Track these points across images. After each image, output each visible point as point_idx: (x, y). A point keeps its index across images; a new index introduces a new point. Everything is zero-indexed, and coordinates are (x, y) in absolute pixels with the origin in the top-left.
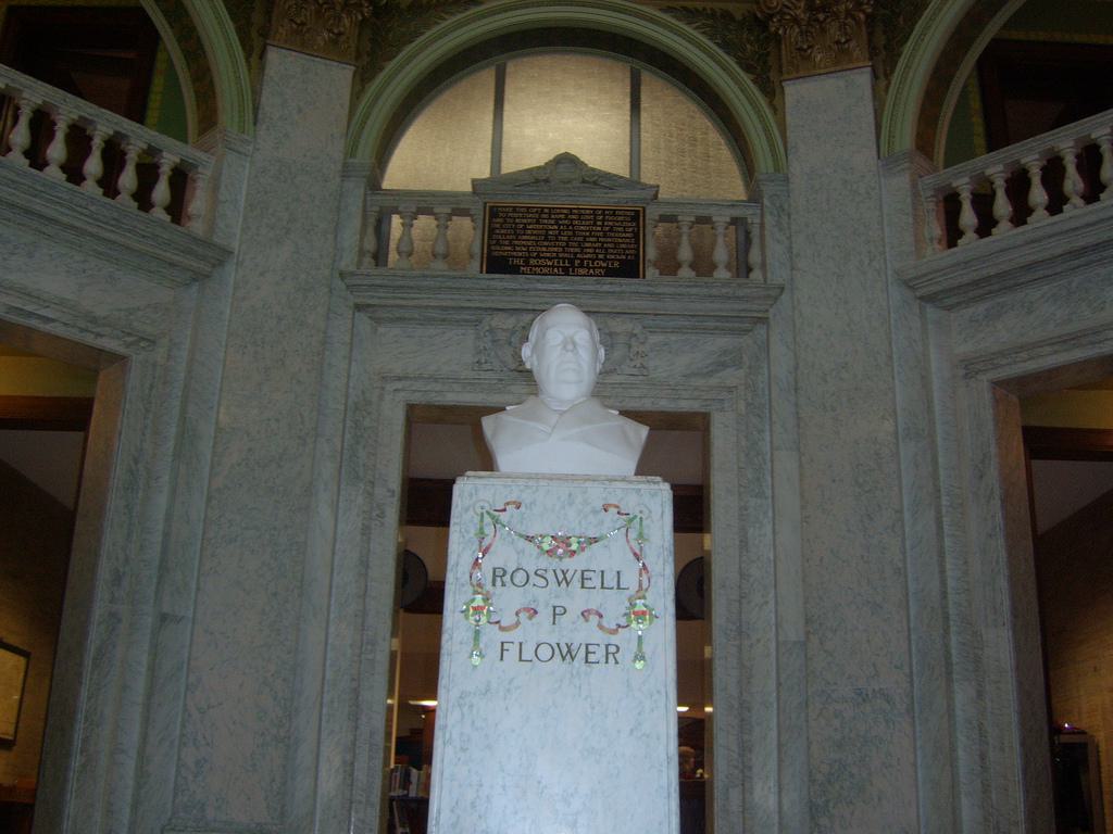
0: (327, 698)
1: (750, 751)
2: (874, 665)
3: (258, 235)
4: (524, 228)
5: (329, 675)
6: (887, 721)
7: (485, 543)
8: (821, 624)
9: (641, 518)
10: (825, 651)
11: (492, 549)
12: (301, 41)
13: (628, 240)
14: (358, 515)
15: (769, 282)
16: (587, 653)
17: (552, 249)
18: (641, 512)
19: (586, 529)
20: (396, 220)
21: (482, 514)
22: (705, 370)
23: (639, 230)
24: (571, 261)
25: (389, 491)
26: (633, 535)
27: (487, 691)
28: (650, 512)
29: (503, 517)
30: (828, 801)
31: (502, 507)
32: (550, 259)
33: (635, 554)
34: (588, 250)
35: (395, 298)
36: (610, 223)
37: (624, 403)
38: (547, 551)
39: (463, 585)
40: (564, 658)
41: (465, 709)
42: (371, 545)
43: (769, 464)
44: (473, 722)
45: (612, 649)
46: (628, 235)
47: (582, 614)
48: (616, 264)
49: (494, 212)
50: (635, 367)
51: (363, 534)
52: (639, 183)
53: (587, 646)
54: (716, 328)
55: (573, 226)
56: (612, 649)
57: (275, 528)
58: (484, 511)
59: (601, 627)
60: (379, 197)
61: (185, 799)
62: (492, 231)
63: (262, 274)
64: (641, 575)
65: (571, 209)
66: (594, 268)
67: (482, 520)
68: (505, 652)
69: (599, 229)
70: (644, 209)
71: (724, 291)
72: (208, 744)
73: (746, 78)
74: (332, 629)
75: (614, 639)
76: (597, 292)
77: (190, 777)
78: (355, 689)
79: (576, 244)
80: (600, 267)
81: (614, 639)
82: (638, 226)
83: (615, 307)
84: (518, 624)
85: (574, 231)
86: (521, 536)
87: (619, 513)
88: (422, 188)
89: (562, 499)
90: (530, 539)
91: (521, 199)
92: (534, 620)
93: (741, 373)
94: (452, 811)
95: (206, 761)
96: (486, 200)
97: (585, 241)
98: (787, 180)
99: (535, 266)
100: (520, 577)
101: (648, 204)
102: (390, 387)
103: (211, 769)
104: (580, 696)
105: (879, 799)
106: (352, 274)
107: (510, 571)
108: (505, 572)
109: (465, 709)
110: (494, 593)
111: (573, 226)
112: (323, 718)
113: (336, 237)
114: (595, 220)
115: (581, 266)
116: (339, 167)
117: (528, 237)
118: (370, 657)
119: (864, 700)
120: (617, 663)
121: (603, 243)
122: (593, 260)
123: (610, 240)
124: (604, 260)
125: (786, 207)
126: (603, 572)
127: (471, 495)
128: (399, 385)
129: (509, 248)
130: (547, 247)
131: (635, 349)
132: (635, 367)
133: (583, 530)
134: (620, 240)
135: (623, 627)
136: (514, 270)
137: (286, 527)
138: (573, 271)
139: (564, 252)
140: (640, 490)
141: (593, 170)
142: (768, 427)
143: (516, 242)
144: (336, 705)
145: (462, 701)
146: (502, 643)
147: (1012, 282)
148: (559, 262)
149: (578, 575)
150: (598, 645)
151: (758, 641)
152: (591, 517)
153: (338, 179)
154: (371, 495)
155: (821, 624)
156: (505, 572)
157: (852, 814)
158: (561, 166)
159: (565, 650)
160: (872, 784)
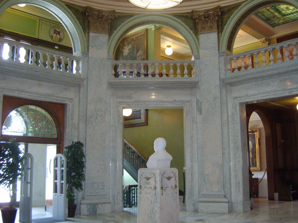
12: (97, 31)
73: (191, 32)
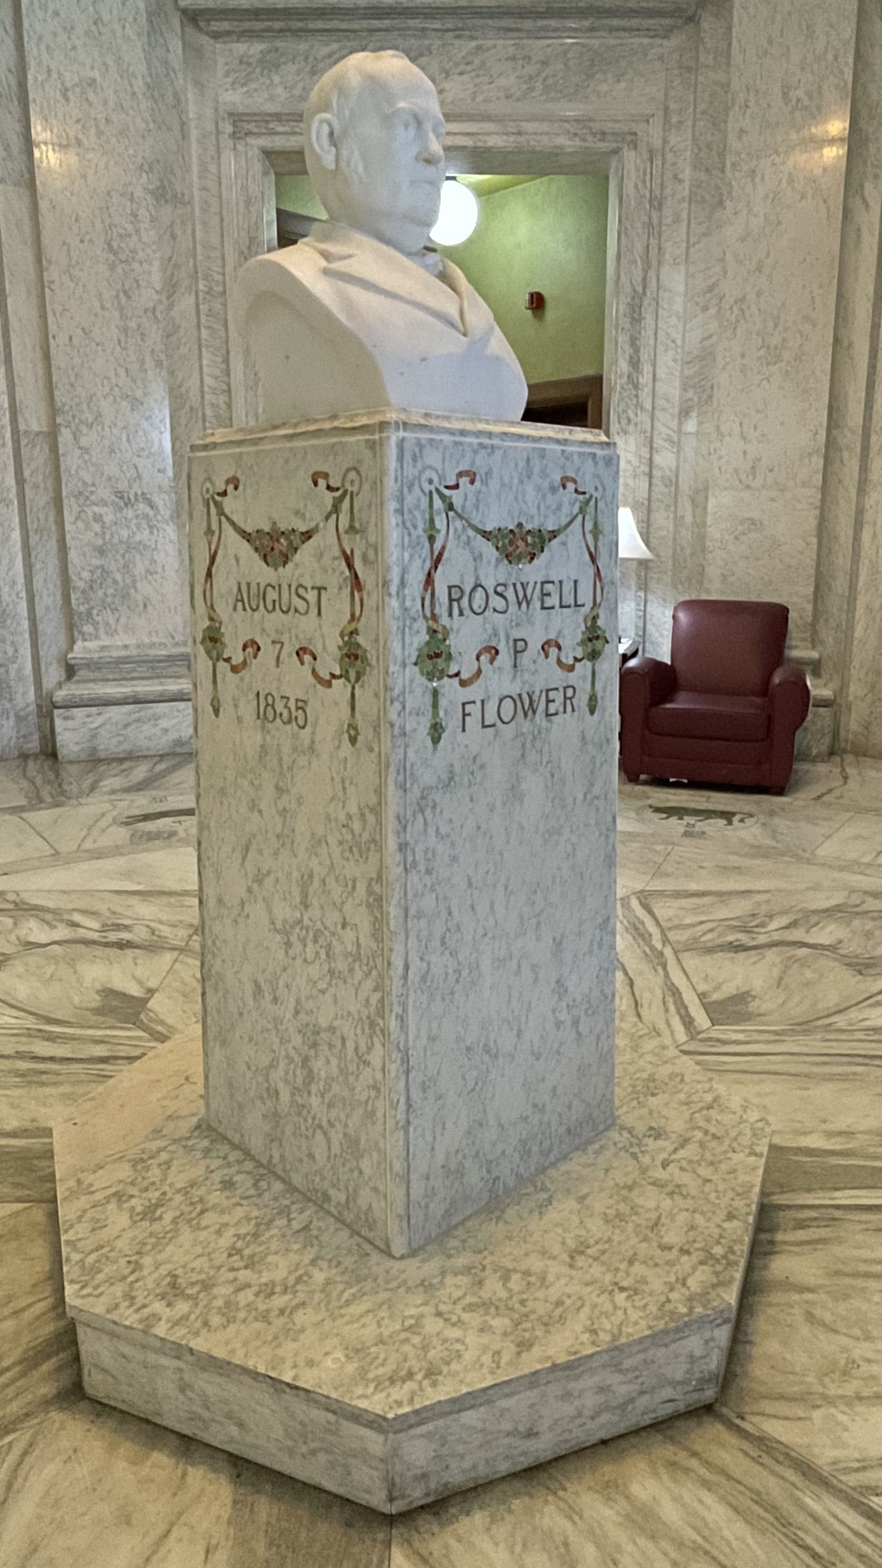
2: (136, 467)
6: (150, 527)
8: (74, 417)
10: (80, 448)
11: (446, 554)
27: (451, 779)
30: (92, 608)
33: (591, 554)
39: (414, 619)
41: (428, 812)
44: (437, 831)
45: (570, 693)
84: (479, 671)
94: (421, 959)
105: (145, 606)
107: (467, 590)
126: (561, 582)
145: (423, 803)
146: (464, 704)
147: (300, 25)
155: (74, 417)
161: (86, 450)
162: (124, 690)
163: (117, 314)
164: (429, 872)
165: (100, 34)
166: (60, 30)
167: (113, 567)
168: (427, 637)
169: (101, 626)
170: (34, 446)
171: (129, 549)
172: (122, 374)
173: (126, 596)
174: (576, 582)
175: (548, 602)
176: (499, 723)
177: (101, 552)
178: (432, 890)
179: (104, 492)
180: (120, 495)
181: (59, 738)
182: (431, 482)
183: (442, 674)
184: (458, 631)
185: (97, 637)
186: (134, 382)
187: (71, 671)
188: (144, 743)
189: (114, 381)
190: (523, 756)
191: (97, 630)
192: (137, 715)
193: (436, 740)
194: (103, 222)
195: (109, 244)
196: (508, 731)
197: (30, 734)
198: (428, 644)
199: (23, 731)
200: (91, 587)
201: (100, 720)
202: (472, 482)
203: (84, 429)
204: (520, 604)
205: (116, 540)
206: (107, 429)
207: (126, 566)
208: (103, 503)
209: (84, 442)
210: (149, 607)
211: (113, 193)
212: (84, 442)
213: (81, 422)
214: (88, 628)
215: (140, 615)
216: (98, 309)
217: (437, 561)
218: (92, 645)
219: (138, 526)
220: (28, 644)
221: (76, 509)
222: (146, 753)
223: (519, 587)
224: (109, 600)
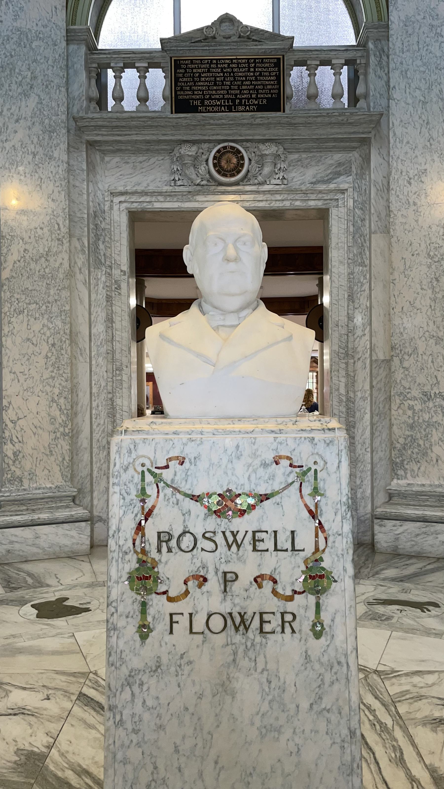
0: (94, 404)
1: (354, 427)
2: (436, 377)
3: (10, 90)
4: (200, 76)
5: (94, 390)
7: (148, 505)
8: (401, 351)
9: (316, 471)
10: (403, 368)
11: (155, 511)
13: (272, 82)
14: (103, 288)
15: (372, 110)
16: (262, 622)
17: (219, 92)
18: (315, 463)
19: (256, 485)
20: (110, 73)
21: (143, 472)
22: (326, 178)
23: (280, 74)
24: (233, 101)
25: (122, 271)
26: (307, 490)
28: (326, 463)
29: (167, 475)
31: (164, 464)
32: (219, 100)
33: (310, 512)
34: (245, 92)
35: (114, 135)
36: (260, 70)
37: (272, 205)
38: (215, 512)
40: (237, 629)
42: (114, 308)
43: (368, 242)
44: (144, 702)
45: (289, 618)
46: (272, 78)
47: (255, 580)
48: (265, 102)
49: (178, 64)
50: (279, 178)
51: (107, 301)
52: (279, 35)
53: (261, 614)
54: (334, 147)
55: (234, 73)
56: (289, 618)
57: (49, 302)
58: (145, 469)
59: (275, 592)
60: (95, 56)
61: (9, 476)
62: (177, 80)
63: (17, 121)
64: (317, 536)
65: (232, 59)
66: (249, 105)
67: (143, 479)
68: (174, 625)
69: (252, 74)
70: (283, 56)
71: (340, 118)
72: (20, 442)
74: (94, 362)
75: (290, 606)
76: (252, 124)
77: (11, 462)
78: (111, 399)
79: (236, 87)
80: (254, 105)
81: (290, 606)
82: (279, 70)
83: (264, 135)
84: (187, 593)
85: (234, 77)
86: (186, 495)
87: (291, 465)
88: (126, 47)
89: (229, 452)
90: (196, 498)
91: (196, 53)
92: (204, 588)
93: (350, 179)
95: (20, 452)
96: (170, 55)
97: (242, 85)
98: (387, 27)
99: (209, 106)
100: (187, 541)
101: (287, 52)
102: (117, 200)
103: (23, 457)
104: (256, 670)
105: (437, 461)
106: (82, 118)
107: (176, 534)
108: (170, 537)
109: (136, 689)
110: (160, 560)
111: (234, 73)
112: (93, 416)
113: (67, 89)
114: (249, 68)
115: (240, 104)
116: (64, 33)
117: (202, 84)
118: (119, 378)
119: (429, 400)
120: (293, 631)
121: (255, 85)
122: (249, 99)
123: (259, 83)
124: (256, 99)
125: (386, 49)
126: (275, 532)
127: (130, 452)
128: (122, 198)
129: (190, 93)
130: (216, 90)
131: (278, 166)
132: (279, 178)
133: (253, 486)
134: (267, 83)
135: (300, 593)
136: (194, 110)
137: (56, 301)
138: (235, 109)
139: (228, 93)
140: (313, 439)
141: (247, 26)
142: (367, 217)
143: (194, 88)
144: (100, 408)
145: (131, 680)
146: (171, 615)
148: (224, 102)
149: (250, 535)
150: (273, 613)
151: (359, 359)
152: (261, 472)
153: (64, 44)
154: (110, 275)
155: (401, 351)
156: (170, 537)
157: (419, 468)
158: (224, 24)
159: (238, 620)
160: (432, 451)
161: (407, 369)
162: (417, 512)
163: (430, 291)
164: (136, 731)
165: (431, 145)
166: (409, 151)
167: (418, 436)
168: (137, 565)
169: (409, 472)
170: (380, 368)
171: (429, 425)
172: (431, 323)
173: (425, 454)
174: (293, 532)
175: (260, 546)
176: (207, 631)
177: (411, 427)
178: (138, 745)
179: (415, 393)
180: (425, 394)
181: (375, 537)
182: (143, 465)
183: (149, 591)
184: (166, 563)
185: (406, 478)
186: (438, 327)
187: (391, 496)
188: (429, 549)
189: (426, 329)
190: (234, 660)
191: (406, 474)
192: (424, 530)
193: (144, 637)
194: (426, 242)
195: (429, 254)
196: (220, 639)
197: (366, 531)
198: (137, 570)
199: (362, 529)
200: (404, 448)
201: (401, 530)
202: (182, 463)
203: (406, 357)
204: (229, 547)
205: (421, 421)
206: (420, 356)
207: (426, 436)
208: (415, 399)
209: (406, 364)
210: (439, 461)
211: (432, 226)
212: (406, 364)
213: (405, 353)
214: (401, 472)
215: (434, 466)
216: (419, 290)
217: (148, 515)
218: (403, 482)
219: (435, 412)
220: (369, 478)
221: (398, 401)
222: (429, 555)
223: (228, 534)
224: (415, 456)
